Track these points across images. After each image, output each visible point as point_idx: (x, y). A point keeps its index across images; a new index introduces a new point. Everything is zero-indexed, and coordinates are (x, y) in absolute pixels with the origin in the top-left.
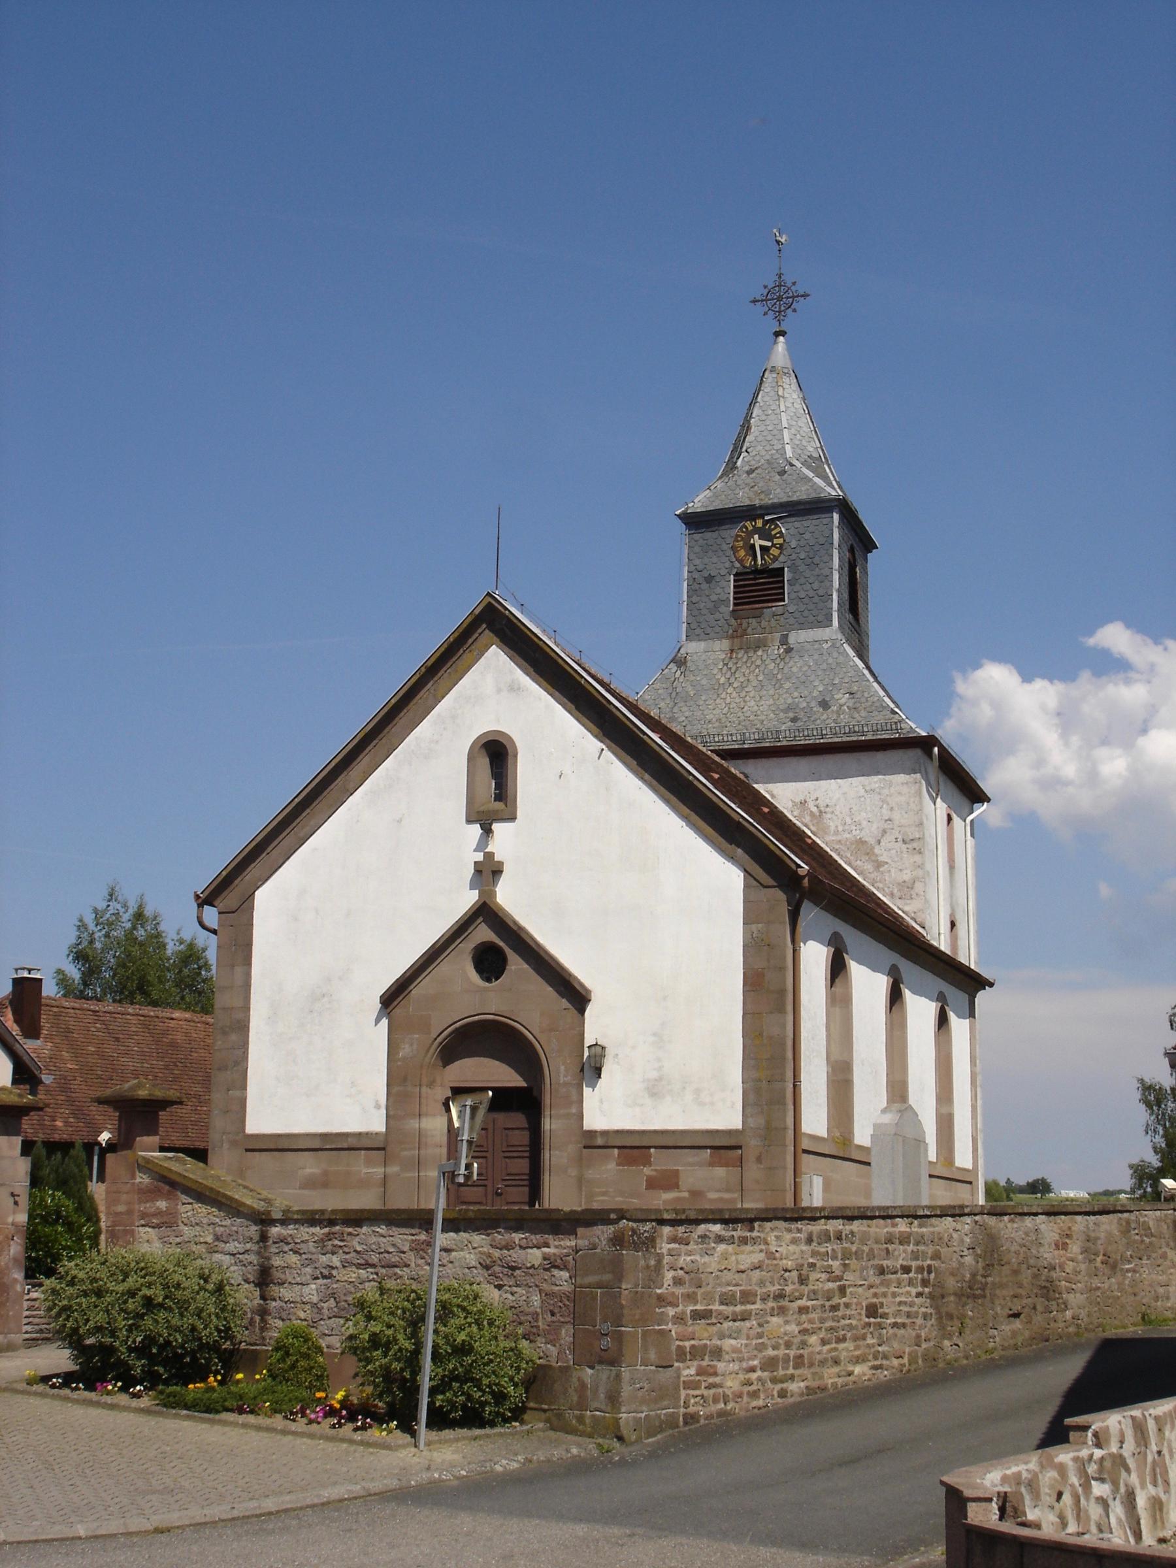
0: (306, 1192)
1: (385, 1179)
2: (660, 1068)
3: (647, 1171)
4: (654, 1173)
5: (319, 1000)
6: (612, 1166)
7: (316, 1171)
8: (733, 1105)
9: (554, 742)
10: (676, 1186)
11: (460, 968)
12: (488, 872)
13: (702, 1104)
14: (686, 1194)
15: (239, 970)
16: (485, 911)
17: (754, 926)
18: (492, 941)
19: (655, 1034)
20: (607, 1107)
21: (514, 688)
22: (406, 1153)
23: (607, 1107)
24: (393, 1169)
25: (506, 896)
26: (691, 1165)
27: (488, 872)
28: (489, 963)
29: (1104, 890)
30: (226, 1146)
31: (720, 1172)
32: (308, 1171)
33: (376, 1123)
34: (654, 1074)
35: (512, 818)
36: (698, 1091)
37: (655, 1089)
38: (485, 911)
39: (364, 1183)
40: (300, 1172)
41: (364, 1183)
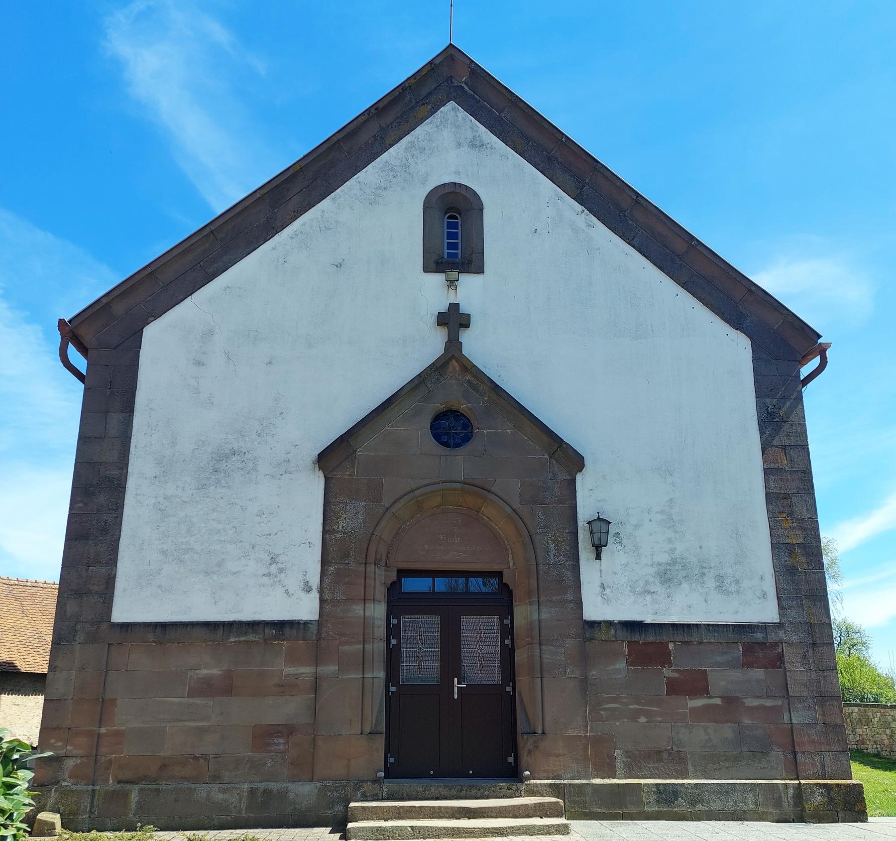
0: (198, 701)
1: (316, 684)
2: (673, 550)
3: (667, 672)
4: (676, 675)
5: (223, 463)
6: (622, 665)
7: (215, 672)
8: (764, 595)
9: (518, 201)
10: (704, 691)
11: (416, 433)
12: (453, 320)
13: (727, 593)
14: (718, 701)
15: (115, 419)
16: (452, 362)
17: (768, 401)
18: (453, 405)
19: (662, 512)
20: (610, 592)
21: (476, 145)
22: (346, 648)
23: (610, 592)
24: (329, 669)
25: (475, 345)
26: (720, 665)
27: (453, 320)
28: (451, 428)
29: (511, 759)
30: (80, 638)
31: (758, 673)
32: (203, 672)
33: (306, 608)
34: (664, 558)
35: (480, 270)
36: (720, 578)
37: (669, 575)
38: (452, 362)
39: (285, 688)
40: (190, 674)
41: (285, 688)
